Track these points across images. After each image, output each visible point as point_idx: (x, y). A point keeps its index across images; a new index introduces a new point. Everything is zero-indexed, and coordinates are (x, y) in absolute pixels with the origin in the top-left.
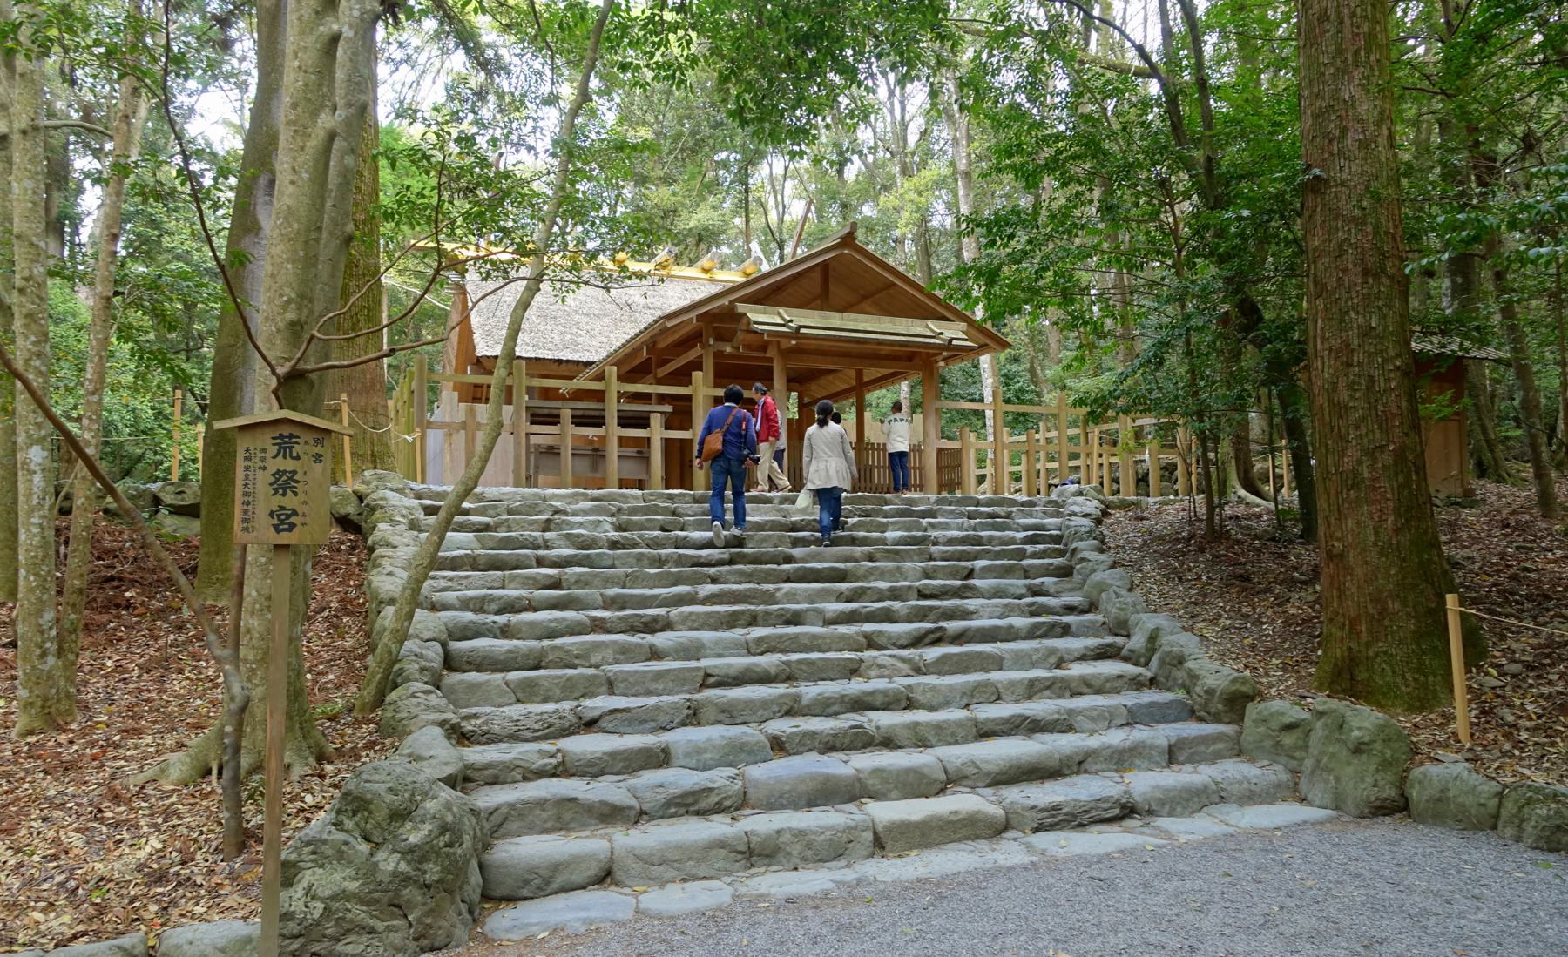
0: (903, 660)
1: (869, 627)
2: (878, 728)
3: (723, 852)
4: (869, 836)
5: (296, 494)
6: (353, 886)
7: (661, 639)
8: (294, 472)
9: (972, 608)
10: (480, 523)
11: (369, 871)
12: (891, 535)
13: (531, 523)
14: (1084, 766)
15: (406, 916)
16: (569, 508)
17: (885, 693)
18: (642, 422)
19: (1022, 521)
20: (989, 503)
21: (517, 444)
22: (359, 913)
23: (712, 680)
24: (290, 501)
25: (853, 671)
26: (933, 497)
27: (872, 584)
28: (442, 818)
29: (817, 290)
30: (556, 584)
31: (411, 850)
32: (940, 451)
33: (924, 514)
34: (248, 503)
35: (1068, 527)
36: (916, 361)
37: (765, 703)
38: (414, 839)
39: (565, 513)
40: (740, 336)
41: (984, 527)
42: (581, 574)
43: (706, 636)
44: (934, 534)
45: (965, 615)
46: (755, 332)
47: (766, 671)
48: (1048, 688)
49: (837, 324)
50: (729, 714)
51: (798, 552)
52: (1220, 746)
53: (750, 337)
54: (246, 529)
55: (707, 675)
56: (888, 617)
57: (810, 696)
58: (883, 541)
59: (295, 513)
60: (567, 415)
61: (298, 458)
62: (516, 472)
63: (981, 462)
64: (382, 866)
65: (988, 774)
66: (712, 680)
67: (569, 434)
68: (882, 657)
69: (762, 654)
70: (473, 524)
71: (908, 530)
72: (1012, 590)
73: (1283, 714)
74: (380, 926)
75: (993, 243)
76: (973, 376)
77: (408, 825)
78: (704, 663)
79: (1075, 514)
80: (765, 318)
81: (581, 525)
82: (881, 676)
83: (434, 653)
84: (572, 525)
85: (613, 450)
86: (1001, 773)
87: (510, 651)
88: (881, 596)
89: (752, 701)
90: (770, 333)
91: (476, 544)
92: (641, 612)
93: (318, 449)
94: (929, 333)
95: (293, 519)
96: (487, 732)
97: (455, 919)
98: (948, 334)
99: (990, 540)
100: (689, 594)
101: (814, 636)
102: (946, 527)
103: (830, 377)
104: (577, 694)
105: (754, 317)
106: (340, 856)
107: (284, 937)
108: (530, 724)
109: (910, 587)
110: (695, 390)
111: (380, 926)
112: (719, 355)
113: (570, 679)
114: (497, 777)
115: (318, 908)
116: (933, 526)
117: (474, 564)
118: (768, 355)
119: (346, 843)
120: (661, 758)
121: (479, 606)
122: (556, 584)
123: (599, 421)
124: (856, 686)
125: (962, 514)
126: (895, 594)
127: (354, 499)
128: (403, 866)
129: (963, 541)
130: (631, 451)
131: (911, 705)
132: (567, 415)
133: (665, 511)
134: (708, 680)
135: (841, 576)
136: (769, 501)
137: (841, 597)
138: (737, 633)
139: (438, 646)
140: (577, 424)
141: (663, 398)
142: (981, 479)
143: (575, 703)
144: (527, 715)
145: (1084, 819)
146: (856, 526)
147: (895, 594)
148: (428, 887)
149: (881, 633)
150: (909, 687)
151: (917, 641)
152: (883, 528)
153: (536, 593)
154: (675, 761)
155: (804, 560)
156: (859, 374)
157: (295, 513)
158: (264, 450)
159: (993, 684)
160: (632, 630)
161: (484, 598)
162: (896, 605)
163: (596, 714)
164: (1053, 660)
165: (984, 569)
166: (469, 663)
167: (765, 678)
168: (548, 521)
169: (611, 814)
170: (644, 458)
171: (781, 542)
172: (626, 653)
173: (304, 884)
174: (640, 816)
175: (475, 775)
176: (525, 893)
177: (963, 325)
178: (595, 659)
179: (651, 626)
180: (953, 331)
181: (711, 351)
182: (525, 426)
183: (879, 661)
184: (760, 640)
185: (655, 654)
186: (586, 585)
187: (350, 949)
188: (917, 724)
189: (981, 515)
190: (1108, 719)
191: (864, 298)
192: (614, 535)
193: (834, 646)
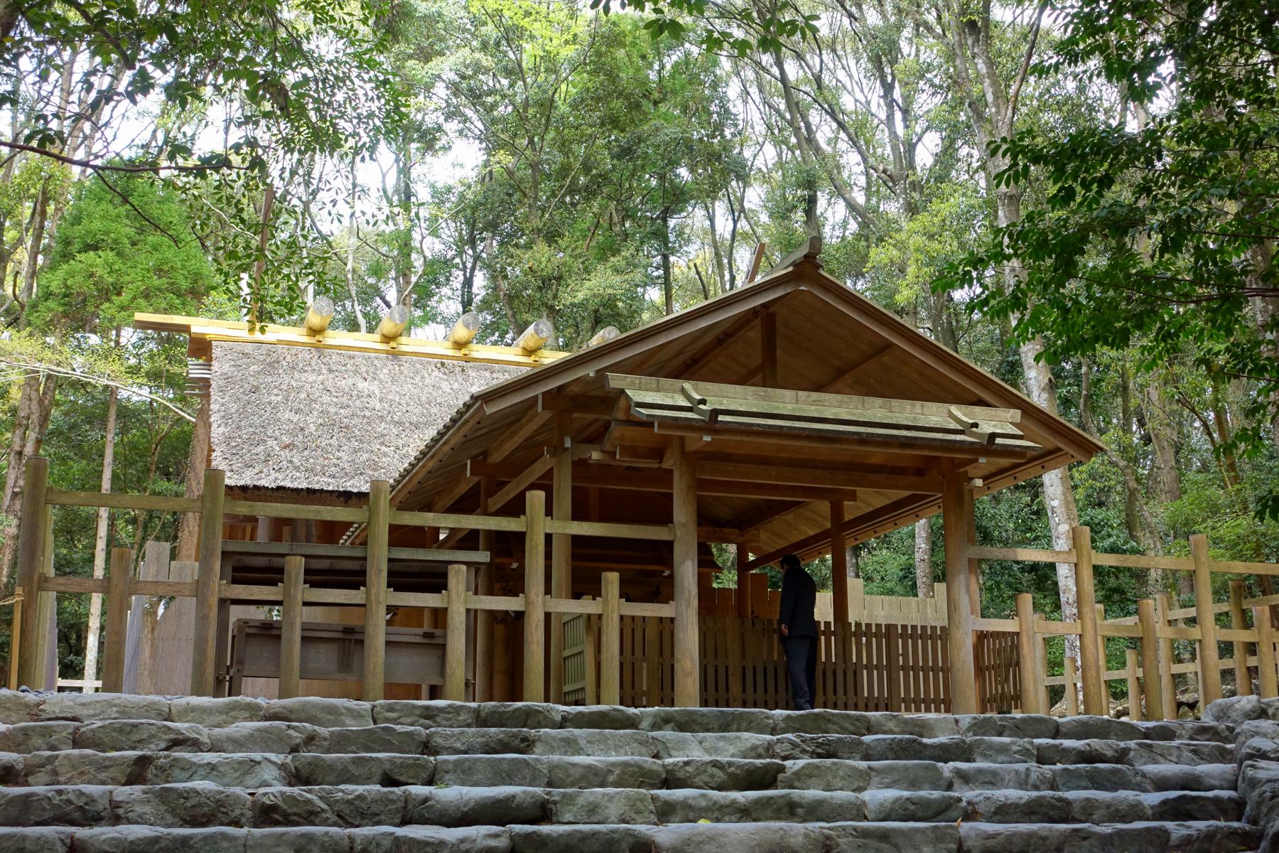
12: (877, 796)
13: (103, 766)
16: (204, 733)
18: (434, 580)
19: (1151, 768)
20: (1082, 731)
21: (202, 619)
26: (966, 719)
29: (757, 359)
32: (982, 637)
33: (945, 753)
35: (1254, 783)
36: (934, 476)
39: (196, 745)
40: (616, 431)
41: (1072, 780)
44: (967, 794)
49: (787, 409)
53: (631, 433)
60: (296, 566)
62: (199, 666)
63: (1054, 665)
67: (301, 606)
71: (913, 785)
75: (1068, 195)
76: (1034, 522)
79: (1263, 755)
80: (654, 396)
84: (191, 770)
85: (378, 633)
90: (665, 422)
94: (953, 425)
98: (986, 428)
99: (1088, 811)
102: (992, 780)
103: (789, 517)
105: (637, 396)
110: (530, 524)
112: (581, 466)
116: (965, 778)
118: (666, 465)
123: (354, 578)
125: (1026, 754)
129: (1030, 811)
130: (411, 634)
132: (296, 566)
133: (406, 742)
136: (632, 723)
140: (314, 585)
141: (469, 540)
142: (1056, 694)
152: (862, 781)
156: (837, 511)
168: (143, 761)
170: (436, 645)
177: (1016, 414)
180: (996, 422)
181: (567, 460)
182: (219, 587)
189: (1064, 755)
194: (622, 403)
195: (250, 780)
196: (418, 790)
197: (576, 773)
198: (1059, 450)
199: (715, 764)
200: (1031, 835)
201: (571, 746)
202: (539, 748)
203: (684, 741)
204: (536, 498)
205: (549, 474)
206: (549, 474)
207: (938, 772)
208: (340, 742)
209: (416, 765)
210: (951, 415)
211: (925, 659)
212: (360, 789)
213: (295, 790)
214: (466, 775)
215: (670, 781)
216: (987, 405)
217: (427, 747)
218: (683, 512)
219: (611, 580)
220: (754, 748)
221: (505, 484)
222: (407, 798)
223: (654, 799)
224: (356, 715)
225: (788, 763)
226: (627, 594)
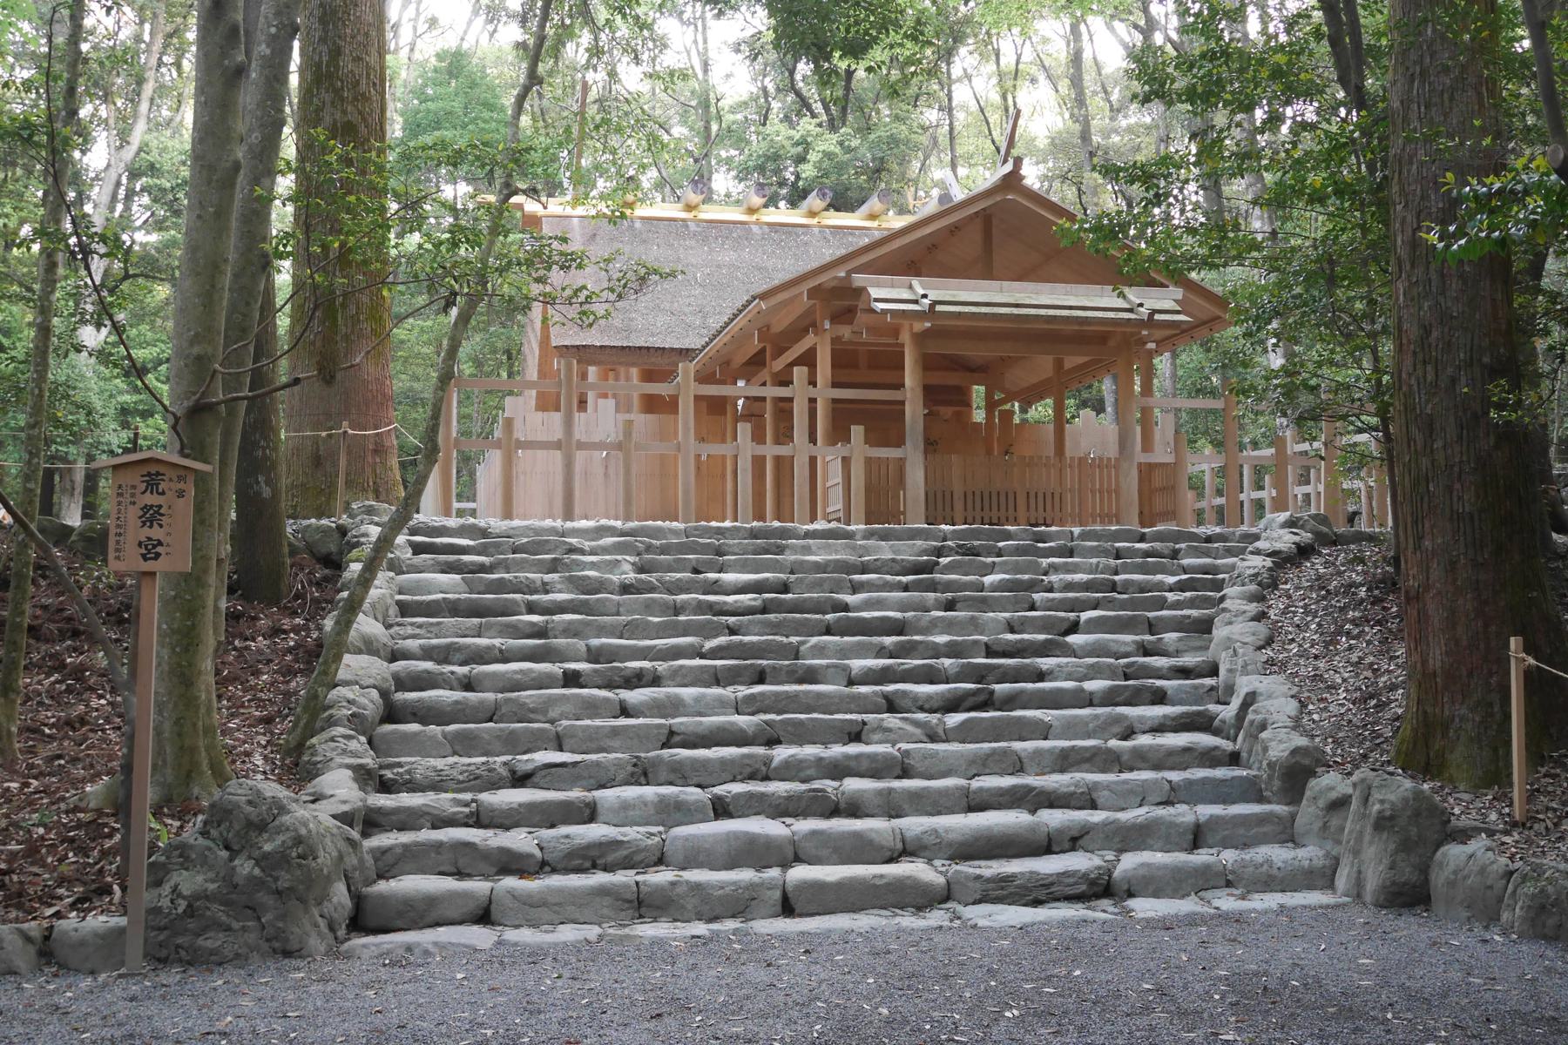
0: (916, 723)
3: (607, 901)
4: (777, 894)
6: (212, 887)
8: (160, 507)
9: (1044, 668)
10: (472, 563)
11: (228, 879)
14: (1080, 842)
15: (259, 919)
16: (587, 545)
22: (217, 911)
24: (156, 533)
25: (856, 736)
28: (296, 830)
31: (266, 856)
38: (267, 847)
42: (570, 622)
45: (1041, 676)
46: (873, 311)
47: (742, 731)
48: (1088, 760)
50: (680, 774)
52: (1267, 829)
54: (118, 558)
55: (672, 733)
59: (160, 543)
61: (163, 493)
64: (238, 869)
65: (950, 844)
68: (891, 720)
70: (465, 564)
72: (1114, 647)
73: (1332, 788)
74: (236, 925)
77: (266, 836)
80: (887, 294)
81: (593, 565)
82: (886, 742)
83: (370, 702)
84: (584, 566)
86: (962, 844)
87: (457, 702)
91: (464, 587)
93: (181, 485)
95: (159, 549)
96: (410, 781)
97: (308, 927)
98: (1151, 304)
100: (692, 645)
106: (204, 862)
107: (153, 928)
108: (455, 773)
111: (236, 925)
112: (835, 341)
114: (407, 820)
115: (182, 905)
117: (454, 609)
119: (209, 849)
120: (589, 814)
121: (443, 655)
122: (541, 632)
127: (336, 535)
128: (257, 871)
133: (704, 549)
137: (881, 652)
139: (374, 693)
144: (452, 767)
145: (1041, 894)
147: (953, 651)
148: (279, 893)
149: (904, 693)
154: (601, 818)
156: (1059, 364)
157: (160, 543)
158: (134, 487)
159: (1015, 753)
161: (449, 647)
163: (530, 767)
164: (1117, 729)
165: (1089, 621)
166: (414, 714)
167: (740, 739)
169: (510, 864)
173: (172, 883)
174: (544, 867)
175: (381, 820)
176: (399, 923)
177: (1178, 293)
178: (552, 714)
183: (885, 724)
185: (625, 711)
187: (209, 944)
190: (1141, 796)
192: (631, 576)
194: (863, 298)
196: (712, 576)
197: (528, 630)
200: (1077, 599)
201: (807, 550)
202: (788, 552)
203: (879, 547)
204: (799, 373)
205: (812, 352)
206: (812, 352)
207: (1038, 565)
208: (664, 550)
209: (710, 562)
211: (1101, 484)
212: (679, 575)
213: (643, 576)
214: (744, 567)
215: (864, 569)
216: (1163, 285)
217: (720, 552)
218: (911, 377)
219: (857, 431)
221: (788, 349)
222: (706, 580)
224: (675, 532)
226: (868, 441)
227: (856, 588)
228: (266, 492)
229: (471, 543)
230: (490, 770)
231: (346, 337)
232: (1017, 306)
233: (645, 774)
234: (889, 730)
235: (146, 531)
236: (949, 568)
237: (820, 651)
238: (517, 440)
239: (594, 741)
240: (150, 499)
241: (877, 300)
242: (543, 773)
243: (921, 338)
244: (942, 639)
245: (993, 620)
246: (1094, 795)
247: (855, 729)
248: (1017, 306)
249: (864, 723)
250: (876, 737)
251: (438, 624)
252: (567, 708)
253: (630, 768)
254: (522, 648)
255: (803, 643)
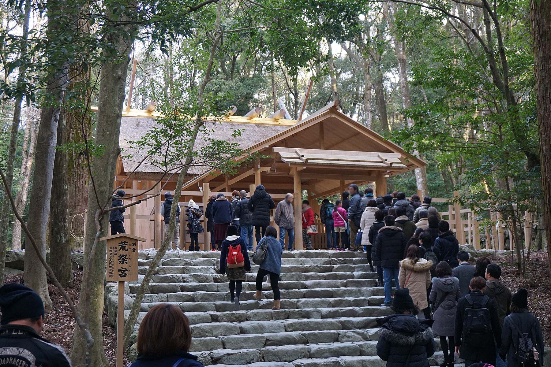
0: (358, 333)
1: (343, 319)
2: (345, 362)
5: (127, 263)
7: (245, 325)
8: (126, 255)
12: (356, 273)
16: (193, 261)
17: (349, 348)
23: (269, 342)
24: (125, 266)
25: (336, 339)
27: (345, 298)
30: (192, 299)
34: (111, 267)
37: (294, 352)
39: (191, 264)
42: (204, 295)
43: (265, 323)
46: (283, 162)
51: (309, 282)
55: (267, 340)
56: (353, 314)
57: (313, 349)
58: (353, 277)
59: (126, 270)
61: (127, 250)
66: (269, 342)
68: (349, 332)
69: (292, 331)
78: (265, 335)
80: (288, 154)
88: (349, 304)
89: (288, 351)
90: (292, 163)
92: (234, 312)
95: (126, 272)
101: (317, 323)
104: (209, 349)
109: (364, 300)
113: (205, 341)
124: (336, 345)
126: (357, 303)
131: (362, 354)
134: (268, 342)
135: (331, 295)
137: (330, 305)
138: (280, 322)
143: (209, 352)
146: (338, 269)
147: (357, 303)
150: (361, 346)
151: (366, 325)
152: (352, 269)
153: (183, 303)
155: (310, 287)
157: (126, 270)
158: (116, 248)
160: (231, 321)
162: (357, 308)
167: (293, 341)
171: (300, 278)
172: (230, 331)
177: (399, 155)
178: (215, 333)
179: (239, 319)
181: (259, 172)
183: (347, 334)
184: (292, 324)
185: (243, 331)
186: (206, 300)
188: (363, 361)
191: (344, 140)
193: (326, 327)
195: (208, 272)
197: (187, 298)
198: (413, 164)
199: (317, 266)
210: (378, 156)
220: (326, 262)
223: (305, 275)
225: (335, 266)
227: (307, 278)
228: (65, 240)
229: (145, 261)
230: (204, 357)
231: (78, 173)
232: (338, 160)
233: (263, 357)
234: (349, 337)
235: (121, 265)
236: (338, 269)
237: (306, 305)
238: (137, 215)
239: (236, 344)
240: (122, 252)
241: (284, 158)
242: (225, 358)
243: (300, 173)
244: (351, 299)
245: (367, 291)
246: (437, 360)
247: (336, 336)
248: (338, 160)
249: (339, 334)
250: (344, 339)
251: (151, 296)
252: (221, 331)
253: (258, 355)
254: (190, 306)
255: (298, 301)
